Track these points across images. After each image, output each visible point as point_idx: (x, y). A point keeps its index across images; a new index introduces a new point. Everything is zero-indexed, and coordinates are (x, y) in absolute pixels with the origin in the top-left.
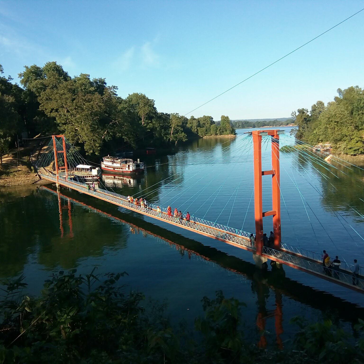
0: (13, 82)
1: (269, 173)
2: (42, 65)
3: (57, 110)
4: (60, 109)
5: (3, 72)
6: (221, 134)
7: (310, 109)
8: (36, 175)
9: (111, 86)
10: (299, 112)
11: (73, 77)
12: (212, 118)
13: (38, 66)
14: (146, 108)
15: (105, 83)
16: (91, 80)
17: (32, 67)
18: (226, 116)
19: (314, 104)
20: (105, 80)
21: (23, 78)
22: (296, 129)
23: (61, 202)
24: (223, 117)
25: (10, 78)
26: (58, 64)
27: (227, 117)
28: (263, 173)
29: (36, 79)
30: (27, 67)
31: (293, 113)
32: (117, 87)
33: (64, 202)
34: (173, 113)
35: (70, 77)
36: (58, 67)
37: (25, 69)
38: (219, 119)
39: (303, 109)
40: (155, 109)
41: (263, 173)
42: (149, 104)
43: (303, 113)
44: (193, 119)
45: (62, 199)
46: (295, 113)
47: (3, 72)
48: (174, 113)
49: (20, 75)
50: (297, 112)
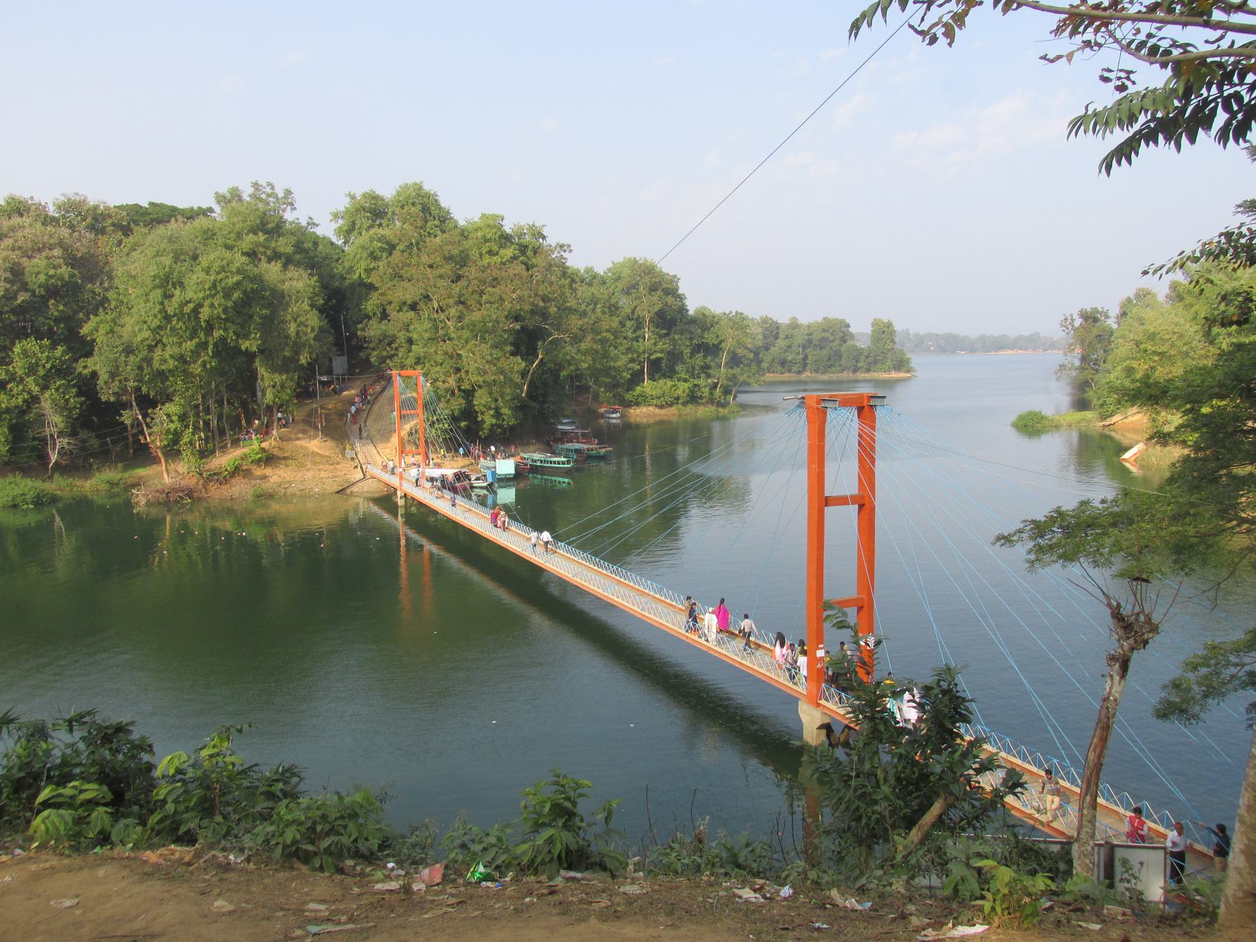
0: (320, 231)
1: (842, 501)
2: (388, 192)
3: (414, 307)
4: (422, 305)
5: (295, 209)
6: (868, 371)
7: (1114, 311)
8: (356, 467)
9: (554, 245)
10: (1082, 316)
11: (462, 223)
12: (848, 326)
13: (380, 192)
14: (655, 298)
15: (544, 238)
16: (508, 228)
17: (364, 196)
18: (885, 321)
19: (1126, 296)
20: (544, 229)
21: (341, 222)
22: (1072, 364)
23: (406, 546)
24: (876, 323)
25: (312, 224)
26: (426, 188)
27: (889, 325)
28: (828, 501)
29: (371, 226)
30: (353, 197)
31: (1066, 320)
32: (569, 246)
33: (414, 547)
34: (727, 312)
35: (456, 222)
36: (427, 196)
37: (348, 200)
38: (868, 330)
39: (1095, 311)
40: (680, 298)
41: (828, 501)
42: (664, 287)
43: (1095, 320)
44: (794, 325)
45: (408, 539)
46: (1073, 320)
47: (295, 209)
48: (731, 312)
49: (336, 216)
50: (1076, 317)
